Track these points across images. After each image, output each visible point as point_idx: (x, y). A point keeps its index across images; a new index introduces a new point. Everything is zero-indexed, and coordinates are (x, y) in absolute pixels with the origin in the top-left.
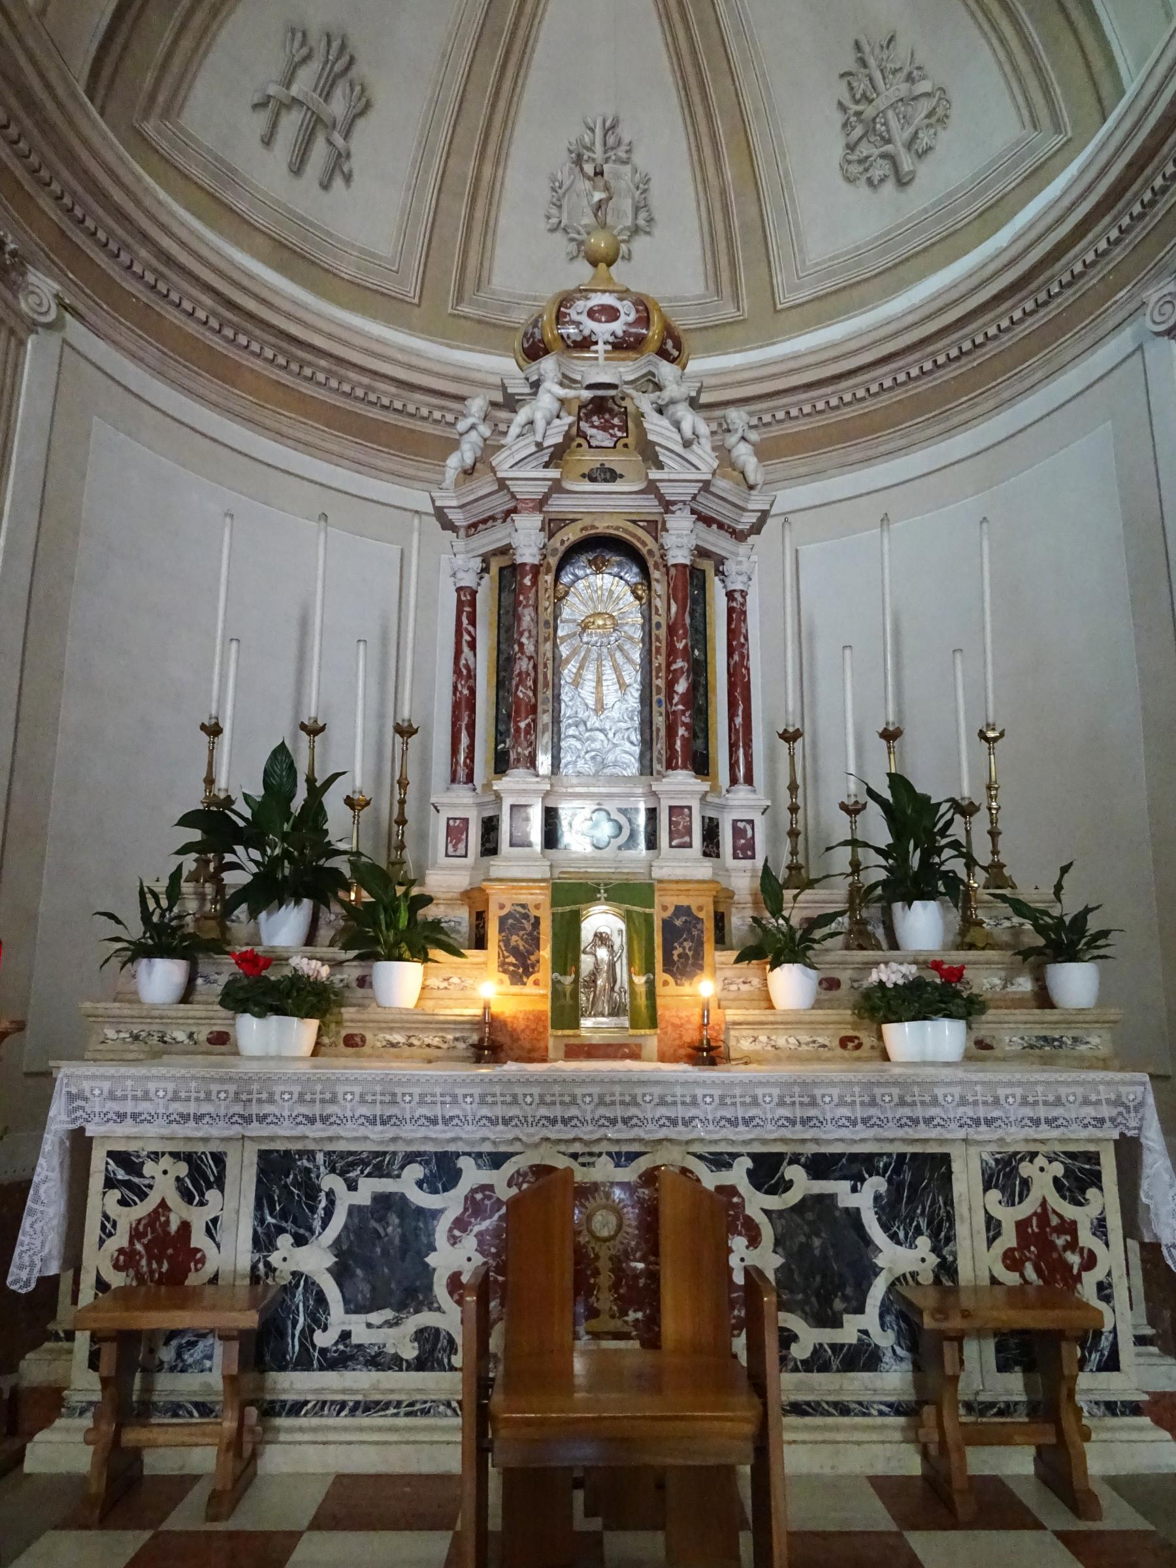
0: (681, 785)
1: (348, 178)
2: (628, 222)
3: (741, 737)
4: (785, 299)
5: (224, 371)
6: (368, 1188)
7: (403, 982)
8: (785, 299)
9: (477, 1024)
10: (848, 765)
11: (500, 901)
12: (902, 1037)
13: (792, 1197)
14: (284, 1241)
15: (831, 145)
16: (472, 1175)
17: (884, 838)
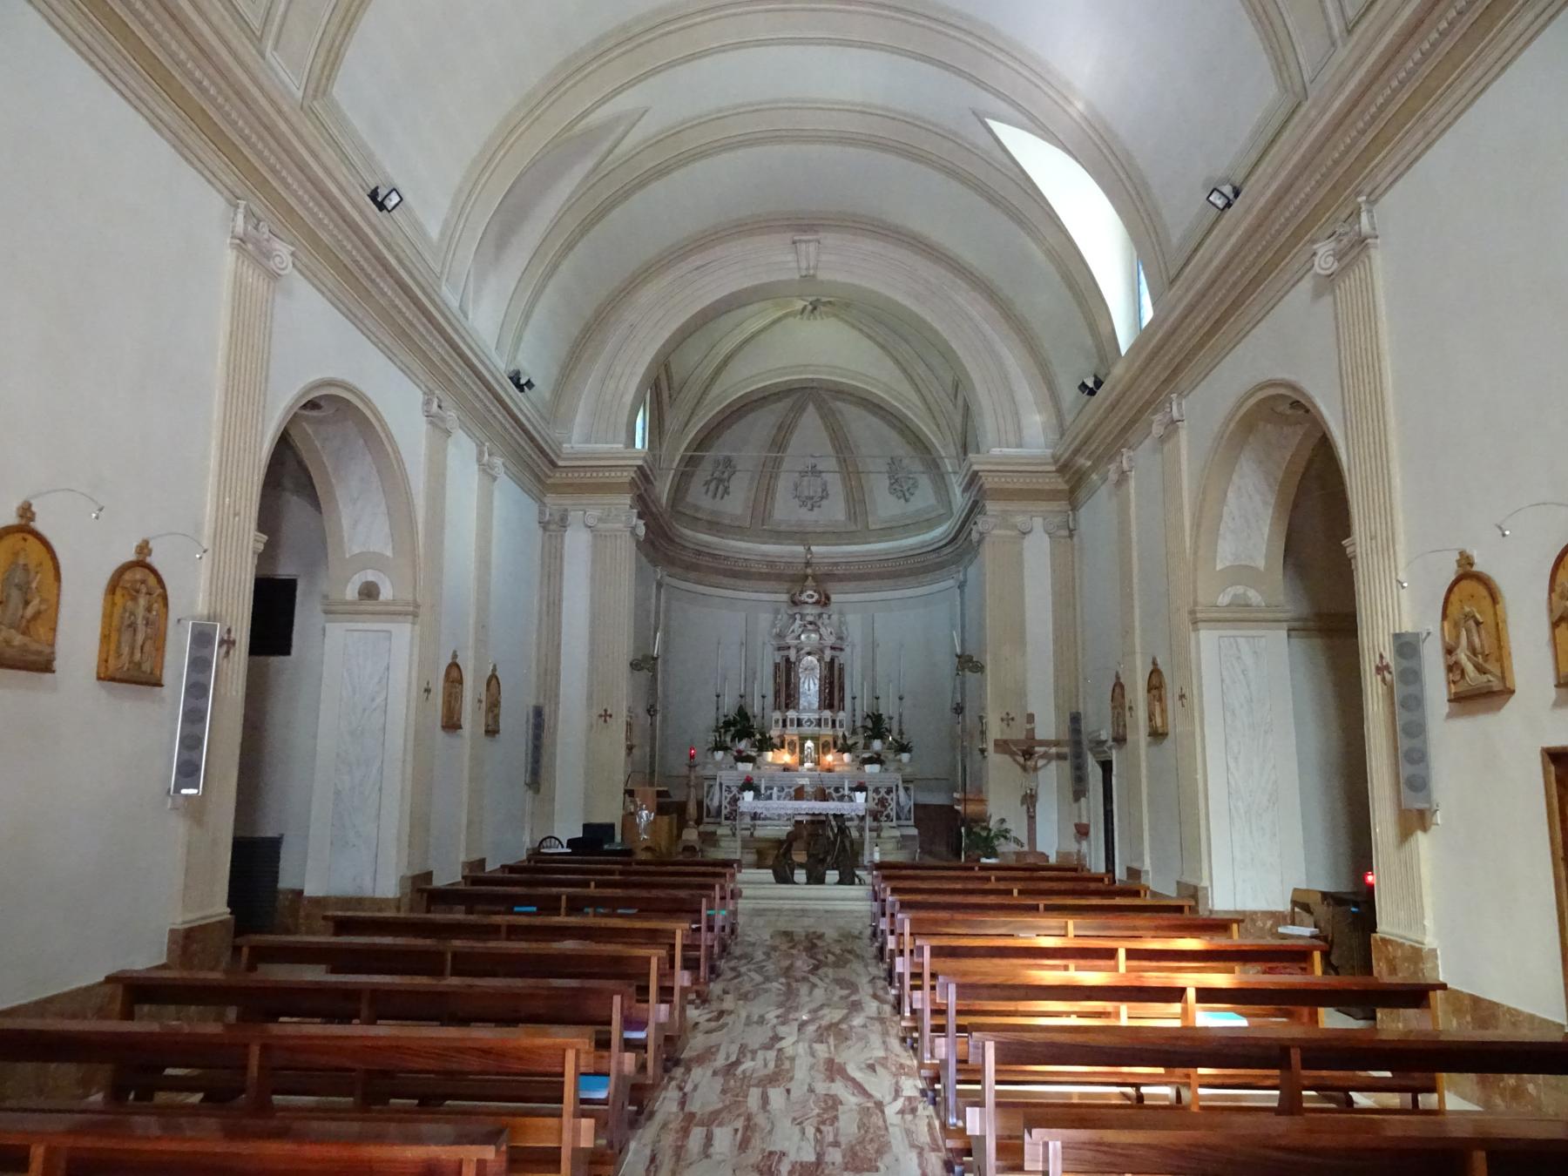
0: (827, 714)
3: (842, 699)
4: (872, 527)
7: (769, 756)
8: (872, 527)
10: (864, 706)
11: (788, 738)
12: (868, 768)
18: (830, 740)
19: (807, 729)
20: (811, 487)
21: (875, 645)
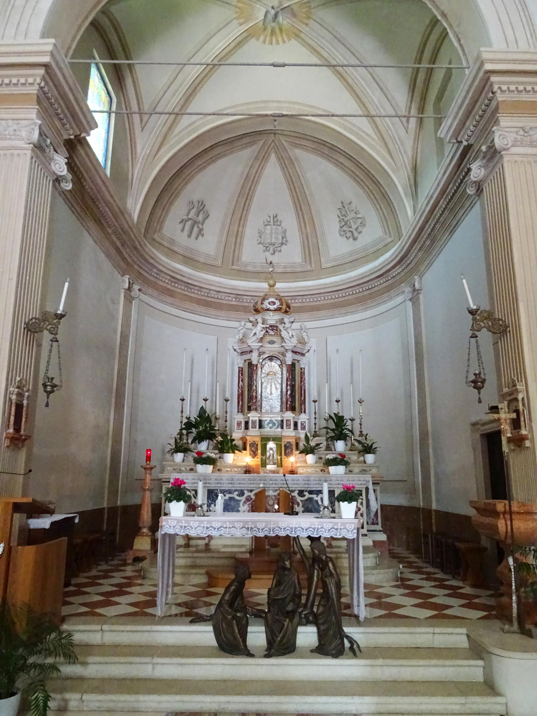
0: (289, 415)
1: (203, 235)
2: (280, 241)
3: (303, 402)
4: (324, 266)
5: (170, 293)
6: (228, 496)
7: (230, 458)
8: (324, 266)
9: (245, 467)
11: (249, 440)
12: (332, 469)
13: (306, 498)
14: (213, 505)
15: (336, 226)
16: (247, 494)
17: (334, 427)
18: (293, 441)
19: (268, 430)
20: (271, 235)
21: (328, 362)
